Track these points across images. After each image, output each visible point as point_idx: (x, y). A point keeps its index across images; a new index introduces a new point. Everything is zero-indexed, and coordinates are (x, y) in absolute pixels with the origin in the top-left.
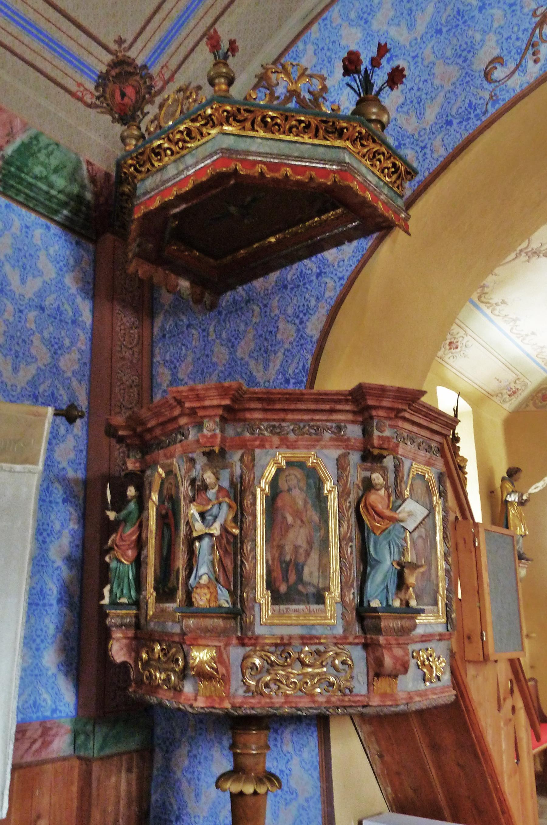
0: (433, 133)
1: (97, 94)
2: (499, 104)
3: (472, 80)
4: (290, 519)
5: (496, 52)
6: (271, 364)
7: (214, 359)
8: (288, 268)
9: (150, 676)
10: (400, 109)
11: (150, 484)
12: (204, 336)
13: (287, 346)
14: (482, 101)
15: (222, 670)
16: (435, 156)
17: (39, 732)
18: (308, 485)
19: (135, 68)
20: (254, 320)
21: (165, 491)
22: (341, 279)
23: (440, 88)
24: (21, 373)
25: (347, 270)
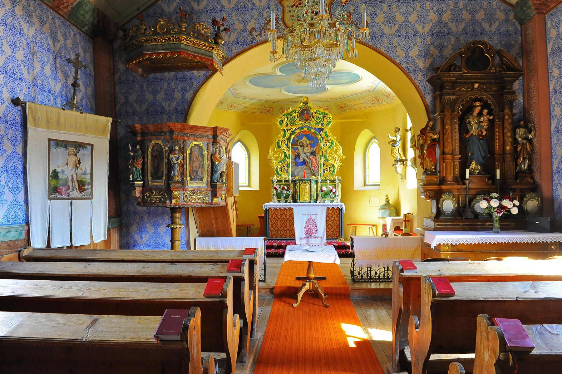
4: (195, 159)
8: (179, 73)
12: (141, 88)
16: (233, 52)
18: (199, 151)
22: (199, 82)
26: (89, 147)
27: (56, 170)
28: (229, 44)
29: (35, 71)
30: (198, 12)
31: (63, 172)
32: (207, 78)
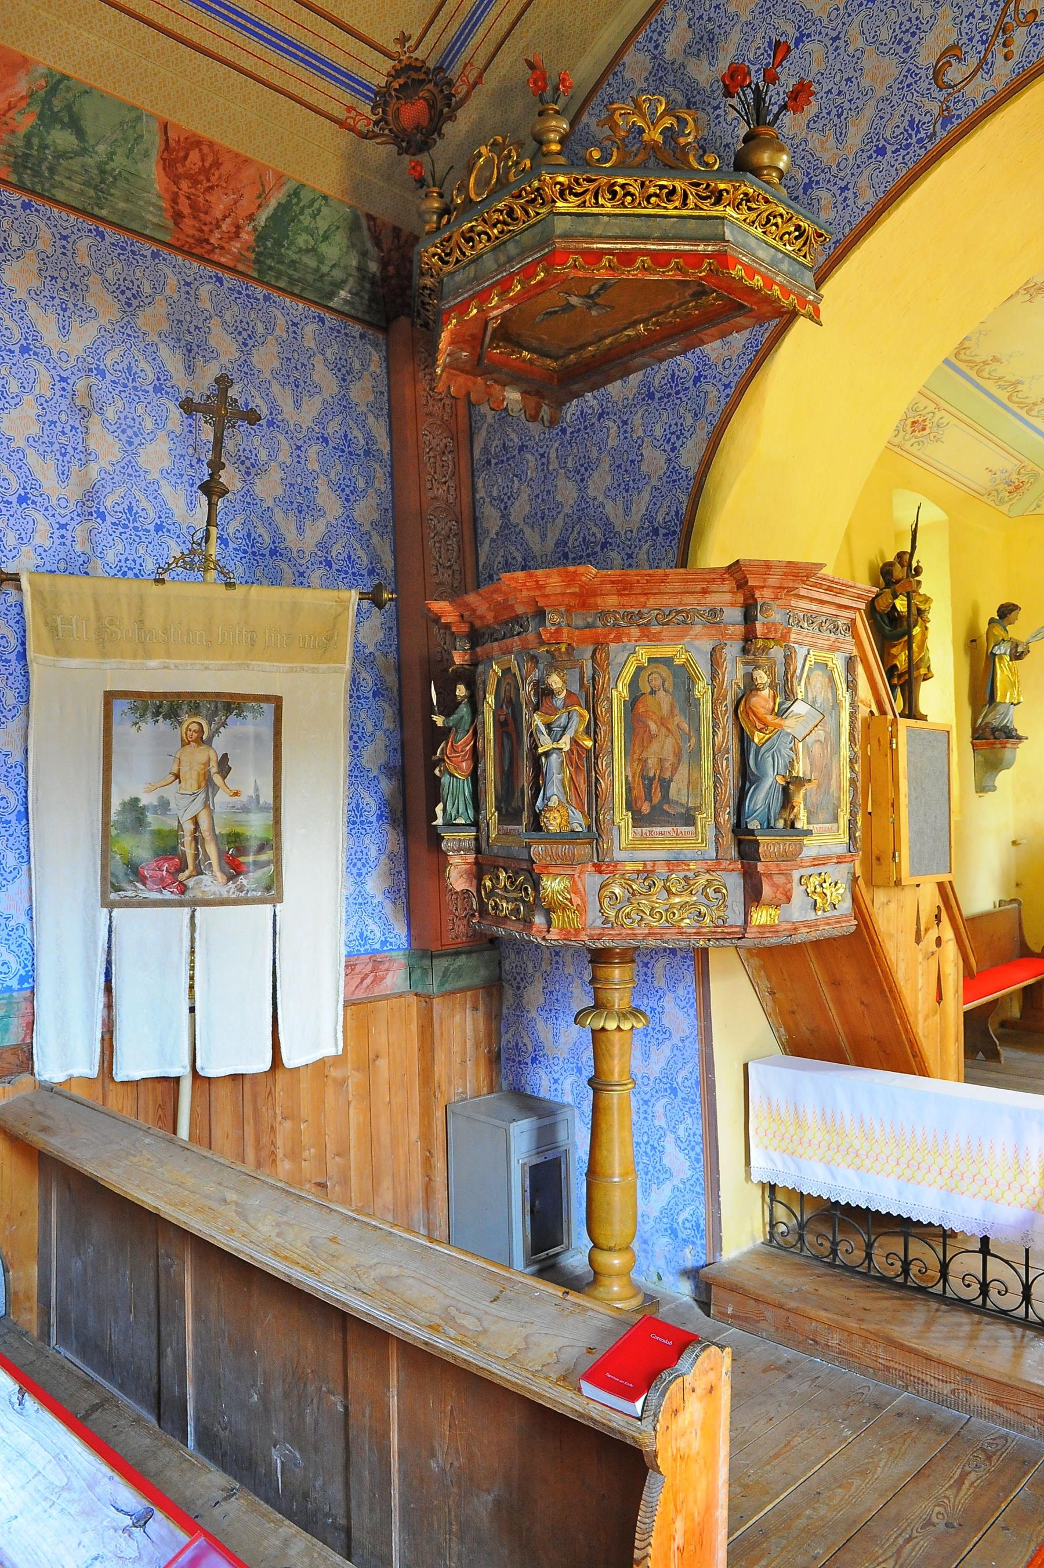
0: (859, 167)
1: (374, 118)
2: (952, 123)
3: (916, 82)
4: (653, 727)
5: (952, 38)
6: (634, 507)
7: (559, 498)
8: (656, 368)
9: (496, 907)
10: (811, 125)
11: (484, 683)
12: (543, 464)
13: (654, 482)
14: (928, 118)
15: (576, 900)
16: (860, 202)
17: (370, 967)
19: (426, 73)
20: (611, 443)
21: (503, 695)
22: (727, 386)
23: (870, 92)
24: (308, 532)
25: (735, 374)
26: (268, 708)
27: (136, 800)
28: (842, 174)
29: (94, 469)
30: (713, 91)
31: (164, 806)
32: (760, 354)
